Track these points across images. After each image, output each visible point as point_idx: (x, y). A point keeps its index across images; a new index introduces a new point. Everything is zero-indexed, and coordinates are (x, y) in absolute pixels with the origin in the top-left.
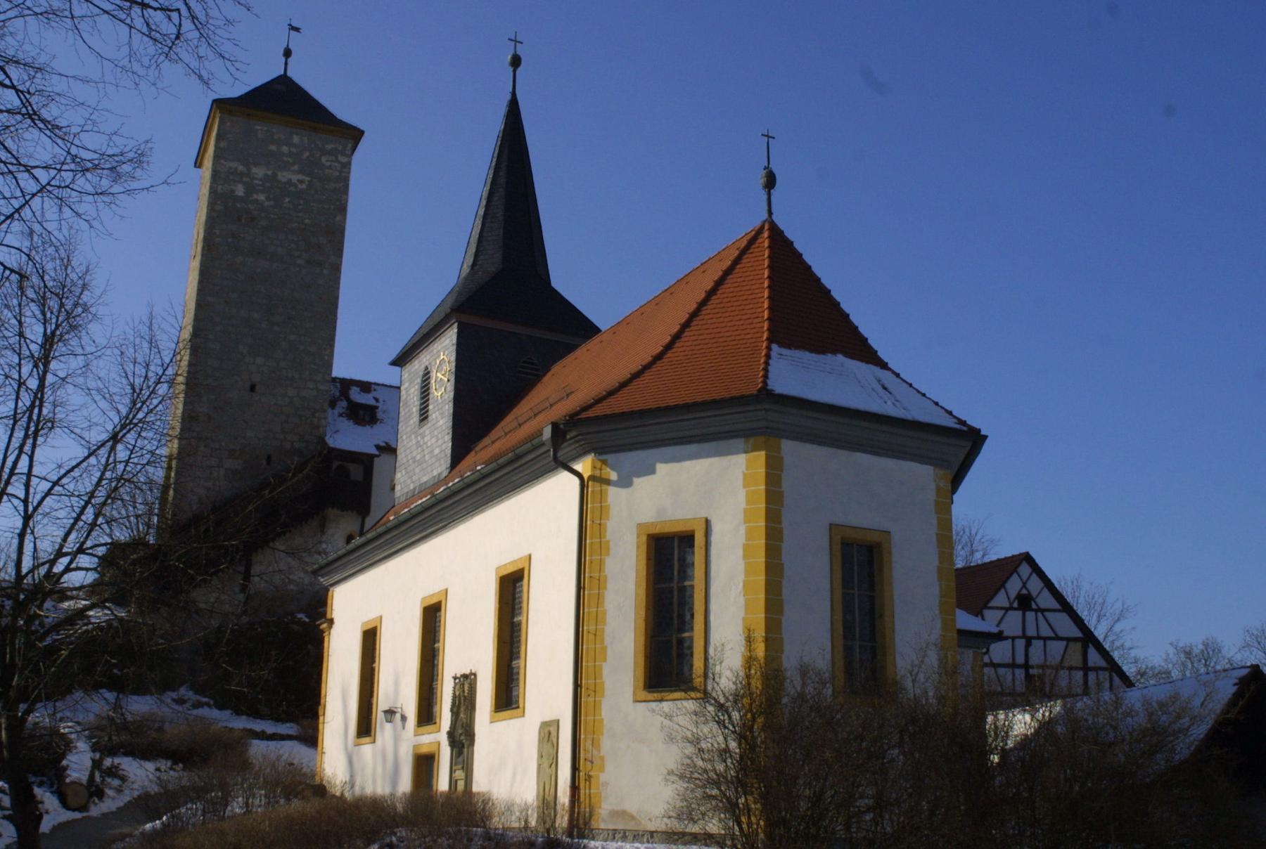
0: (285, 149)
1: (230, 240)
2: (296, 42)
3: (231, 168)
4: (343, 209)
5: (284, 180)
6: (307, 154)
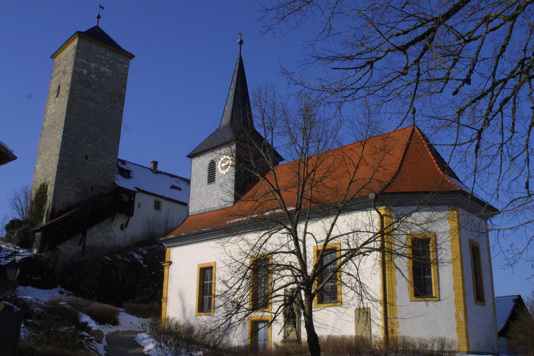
0: (103, 58)
1: (80, 92)
2: (102, 13)
3: (82, 62)
4: (125, 87)
5: (103, 71)
6: (112, 61)
